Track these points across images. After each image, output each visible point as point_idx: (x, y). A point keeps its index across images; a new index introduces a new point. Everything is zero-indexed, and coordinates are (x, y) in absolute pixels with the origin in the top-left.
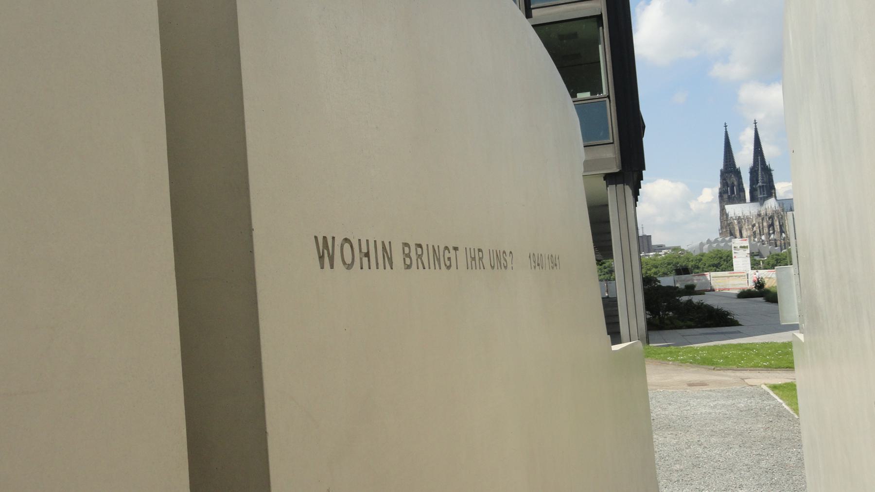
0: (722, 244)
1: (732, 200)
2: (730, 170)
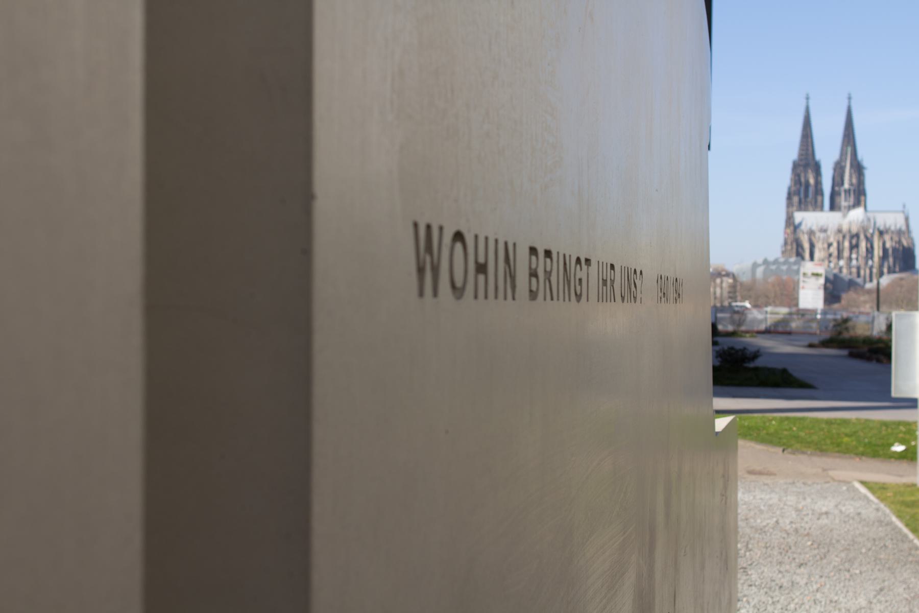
0: (784, 268)
1: (803, 206)
2: (807, 162)
